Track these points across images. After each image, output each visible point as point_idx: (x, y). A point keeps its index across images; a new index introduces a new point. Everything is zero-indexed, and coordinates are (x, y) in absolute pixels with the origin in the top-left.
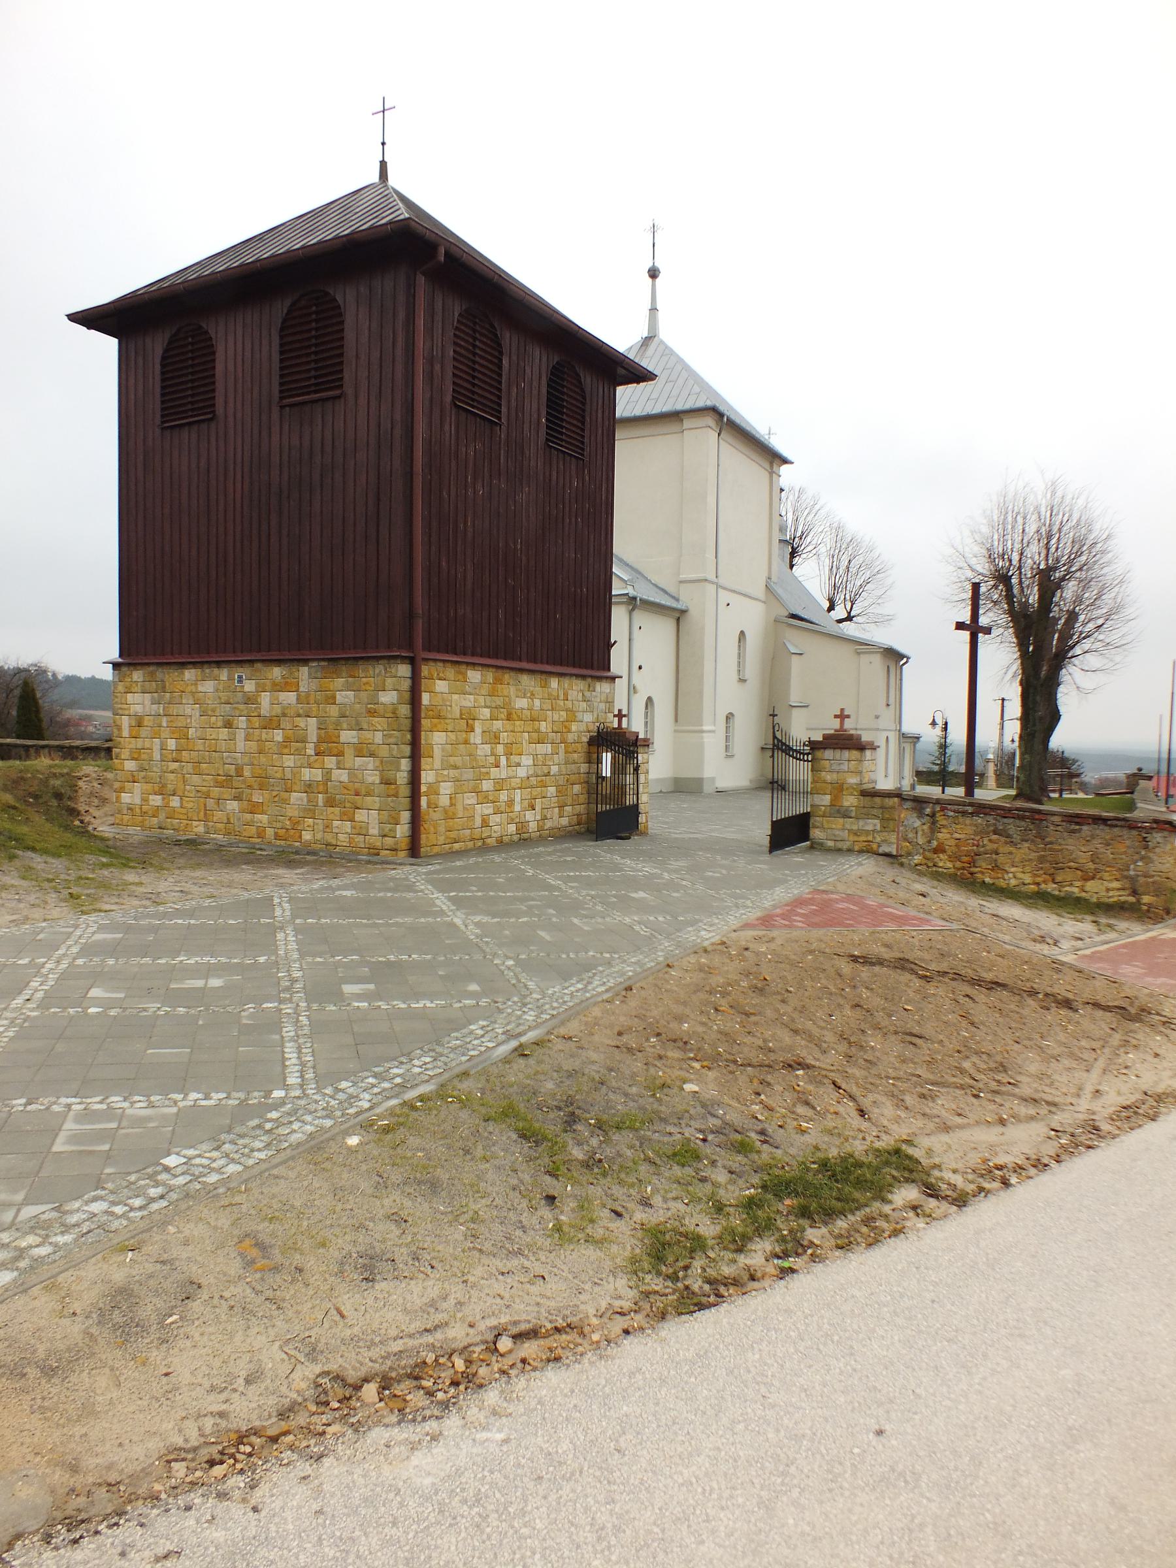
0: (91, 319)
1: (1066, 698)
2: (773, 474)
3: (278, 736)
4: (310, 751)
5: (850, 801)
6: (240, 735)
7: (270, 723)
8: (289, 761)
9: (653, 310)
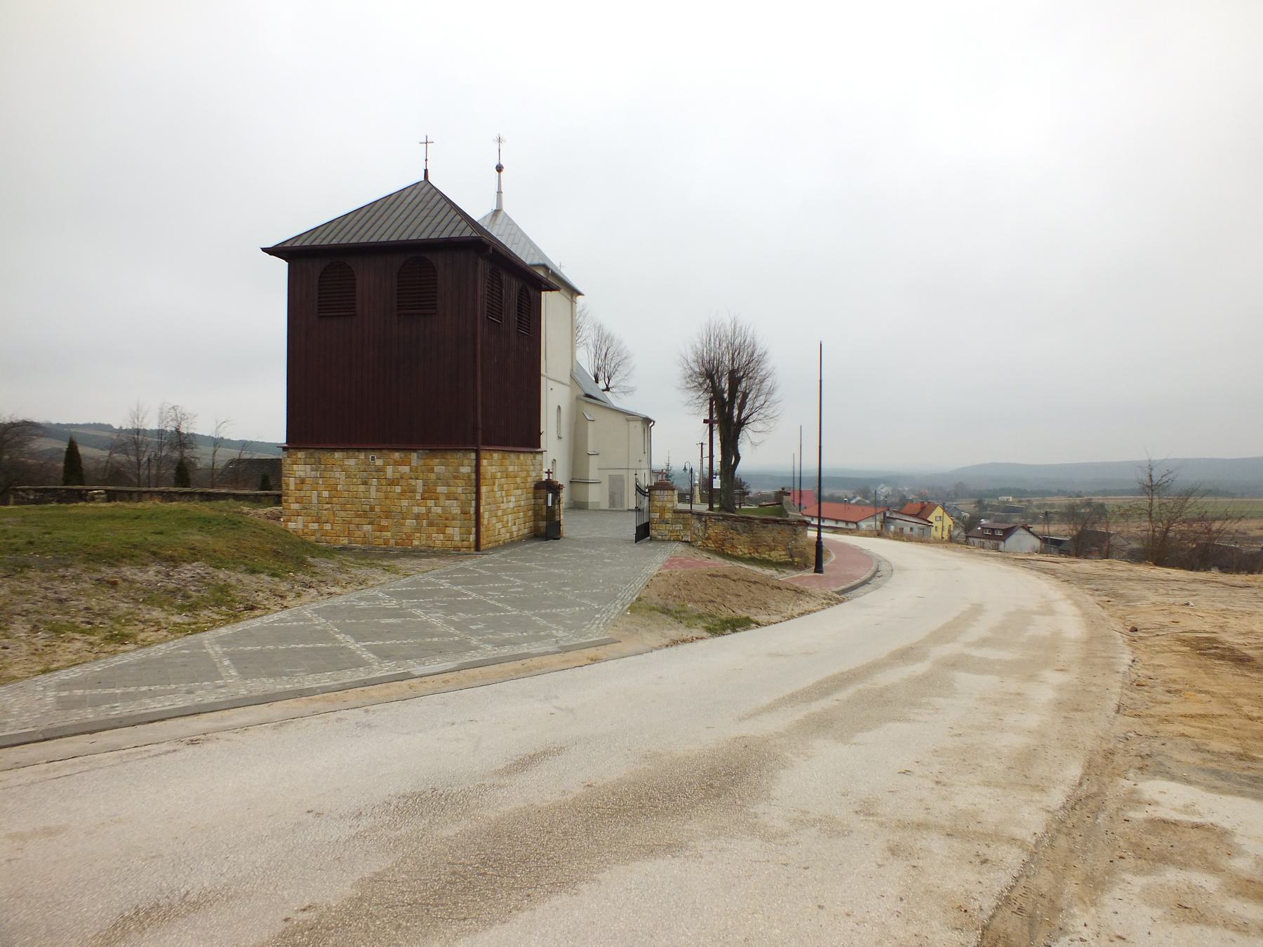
0: (271, 251)
1: (744, 447)
2: (573, 302)
3: (398, 489)
4: (418, 497)
5: (668, 516)
6: (373, 489)
7: (392, 483)
8: (405, 503)
9: (499, 192)
